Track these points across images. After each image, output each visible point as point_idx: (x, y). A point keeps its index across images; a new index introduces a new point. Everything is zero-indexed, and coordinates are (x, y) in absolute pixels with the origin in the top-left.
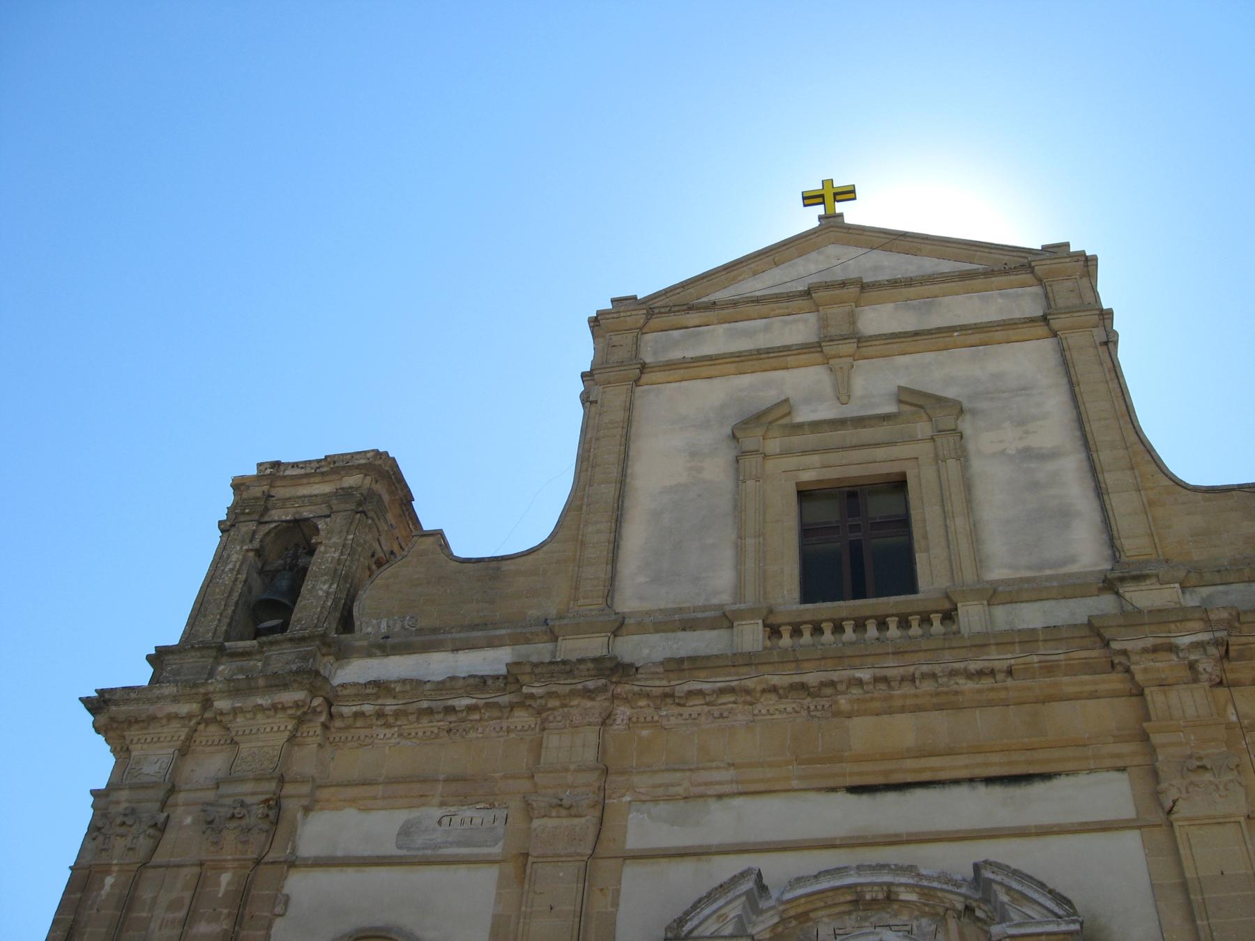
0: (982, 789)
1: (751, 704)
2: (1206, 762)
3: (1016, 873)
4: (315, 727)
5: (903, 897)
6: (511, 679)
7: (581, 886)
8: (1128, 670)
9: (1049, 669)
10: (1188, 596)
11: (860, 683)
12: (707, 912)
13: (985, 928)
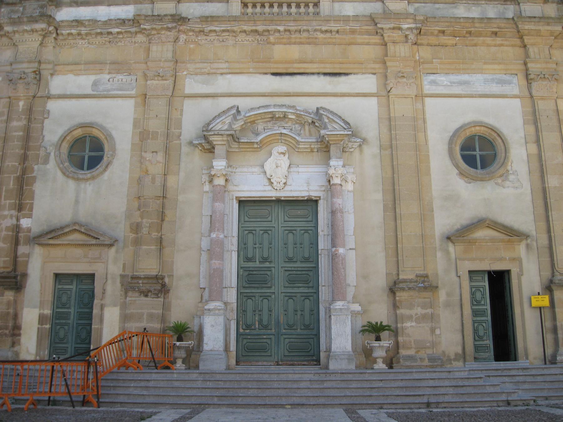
0: (322, 77)
1: (235, 37)
2: (405, 75)
3: (332, 112)
4: (50, 40)
5: (290, 117)
6: (135, 21)
7: (168, 107)
8: (382, 35)
9: (353, 32)
10: (410, 6)
11: (279, 31)
12: (218, 121)
13: (319, 129)
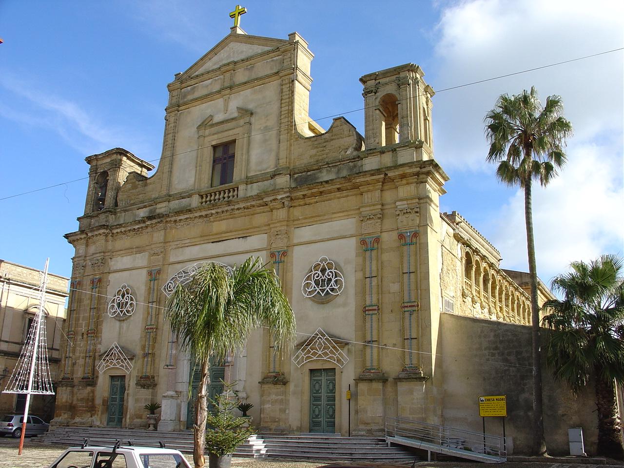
4: (110, 237)
